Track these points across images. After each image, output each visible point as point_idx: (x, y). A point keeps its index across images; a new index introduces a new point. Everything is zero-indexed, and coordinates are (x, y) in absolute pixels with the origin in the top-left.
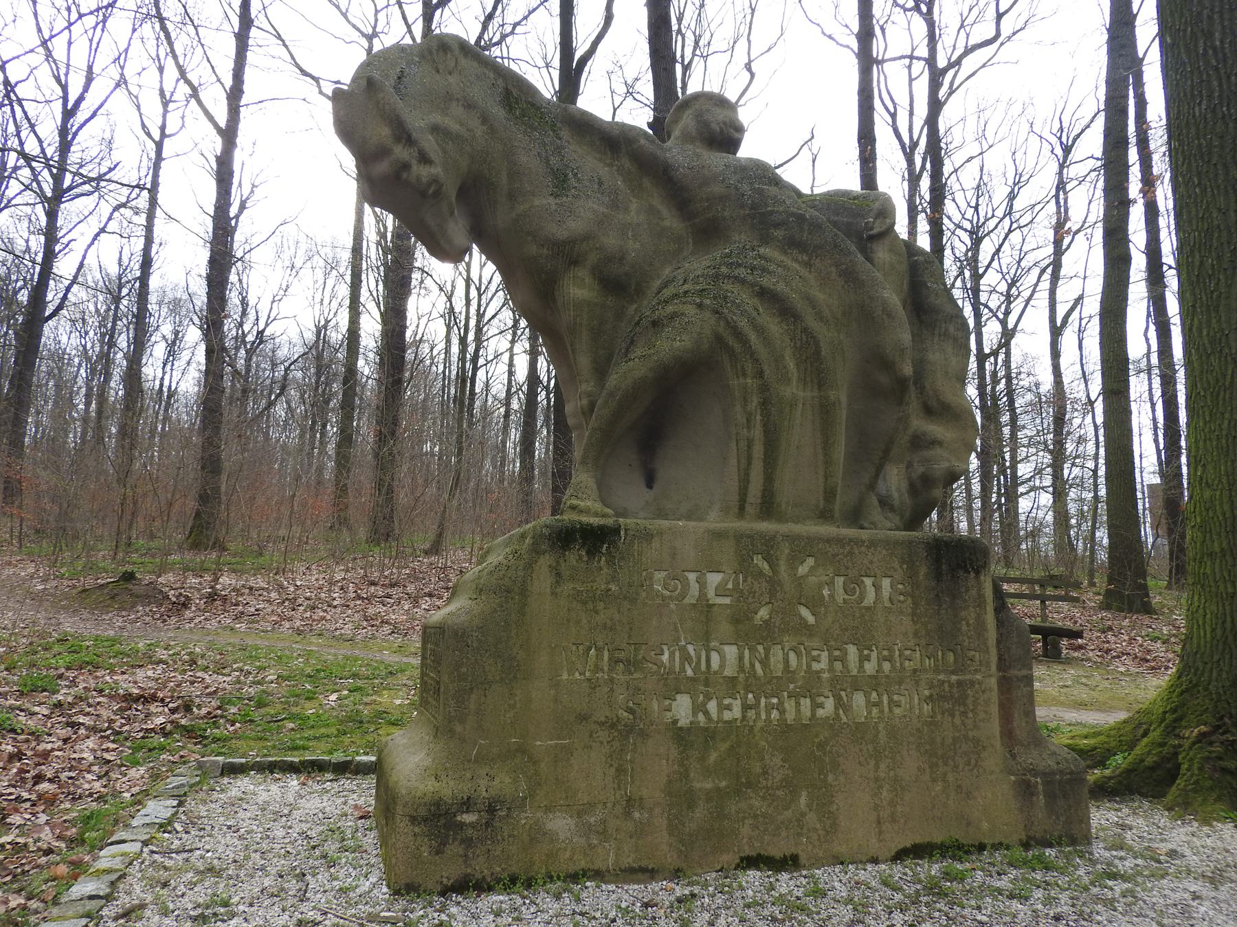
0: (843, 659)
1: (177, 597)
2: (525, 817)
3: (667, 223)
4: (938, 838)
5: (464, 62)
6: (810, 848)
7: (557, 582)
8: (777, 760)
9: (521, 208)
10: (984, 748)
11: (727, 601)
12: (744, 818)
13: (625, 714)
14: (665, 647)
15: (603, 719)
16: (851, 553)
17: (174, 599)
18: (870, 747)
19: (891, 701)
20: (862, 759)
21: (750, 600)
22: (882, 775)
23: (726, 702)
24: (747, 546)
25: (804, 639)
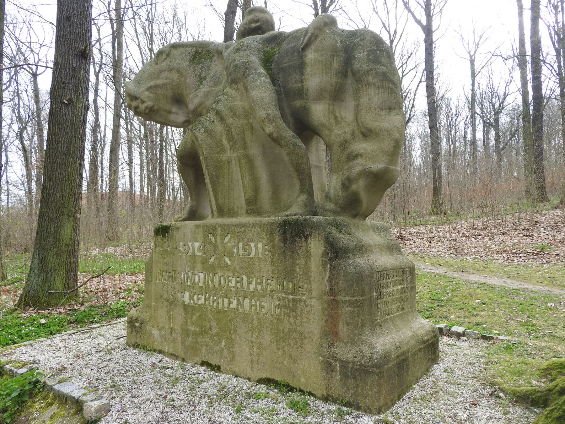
4: (278, 378)
5: (174, 51)
8: (215, 324)
10: (305, 338)
16: (245, 231)
19: (260, 304)
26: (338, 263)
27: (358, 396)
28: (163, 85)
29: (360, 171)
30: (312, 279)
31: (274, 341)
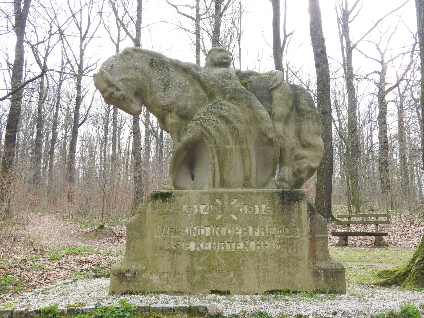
0: (247, 231)
1: (119, 234)
2: (144, 275)
3: (201, 94)
4: (281, 289)
5: (135, 54)
6: (234, 289)
8: (223, 262)
11: (207, 213)
14: (187, 228)
15: (167, 249)
16: (250, 197)
17: (117, 235)
18: (256, 259)
19: (264, 244)
20: (253, 262)
21: (214, 213)
23: (206, 244)
24: (213, 197)
28: (131, 79)
30: (303, 225)
31: (277, 265)
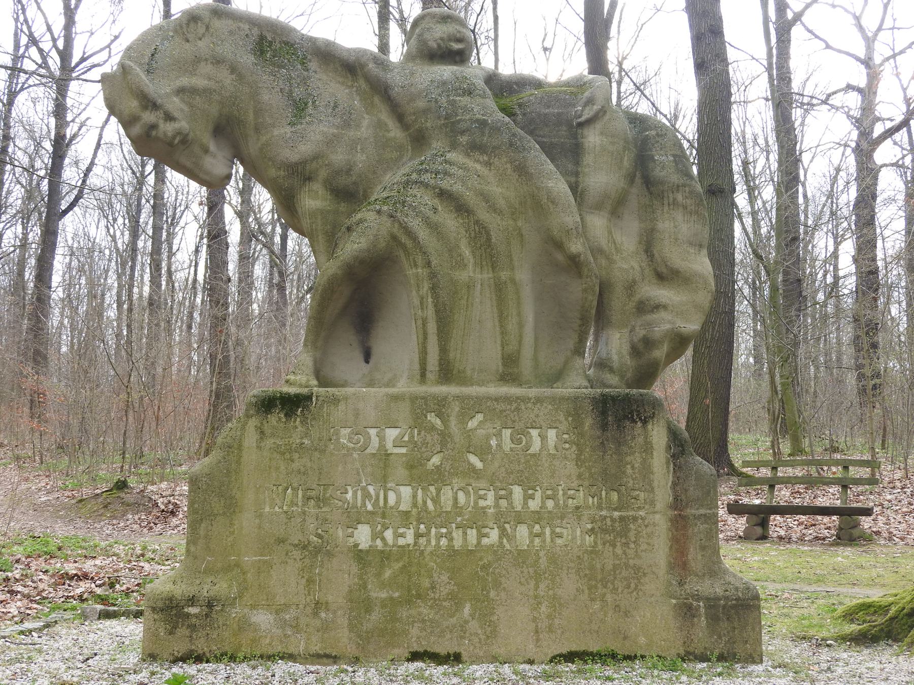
0: (509, 496)
1: (166, 505)
2: (235, 612)
3: (392, 134)
4: (594, 648)
7: (261, 438)
8: (445, 578)
9: (264, 139)
10: (645, 574)
11: (403, 450)
12: (414, 622)
13: (315, 539)
14: (349, 488)
15: (296, 542)
16: (518, 409)
17: (163, 507)
18: (531, 570)
19: (553, 532)
20: (523, 580)
21: (423, 449)
22: (542, 593)
23: (401, 530)
24: (420, 407)
25: (472, 481)
26: (686, 462)
27: (734, 643)
29: (668, 331)
30: (656, 484)
31: (585, 588)
